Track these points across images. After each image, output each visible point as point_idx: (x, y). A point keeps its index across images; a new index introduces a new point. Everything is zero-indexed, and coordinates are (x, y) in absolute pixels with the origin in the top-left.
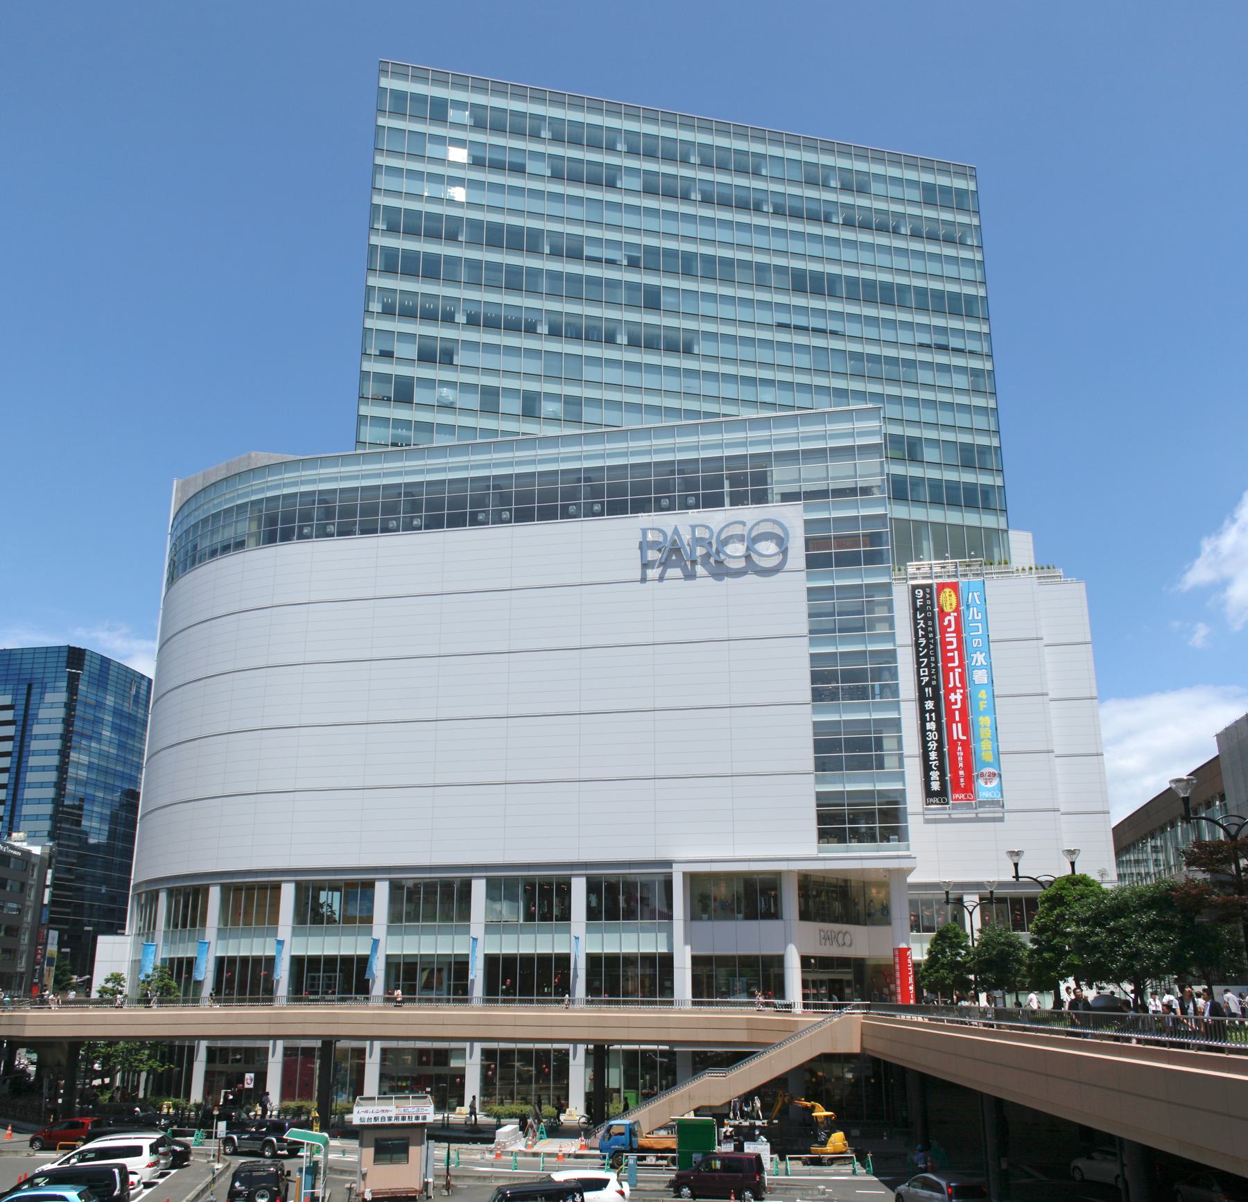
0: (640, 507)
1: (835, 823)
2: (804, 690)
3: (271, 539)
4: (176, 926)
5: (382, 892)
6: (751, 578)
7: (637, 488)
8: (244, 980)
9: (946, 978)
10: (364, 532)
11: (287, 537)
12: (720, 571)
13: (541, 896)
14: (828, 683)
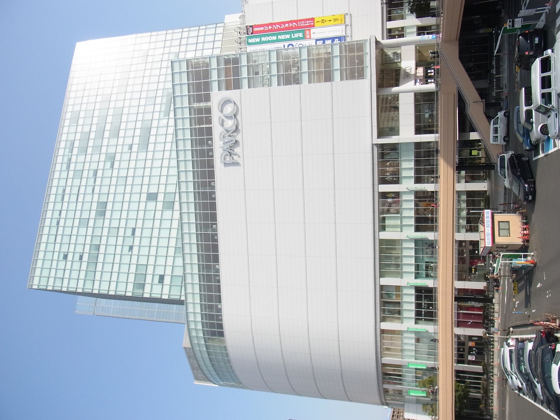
0: (211, 164)
1: (355, 72)
2: (294, 87)
3: (221, 334)
4: (400, 380)
5: (385, 281)
6: (238, 117)
7: (352, 63)
8: (425, 297)
9: (524, 156)
10: (219, 291)
11: (221, 326)
12: (237, 130)
13: (387, 203)
14: (290, 78)
